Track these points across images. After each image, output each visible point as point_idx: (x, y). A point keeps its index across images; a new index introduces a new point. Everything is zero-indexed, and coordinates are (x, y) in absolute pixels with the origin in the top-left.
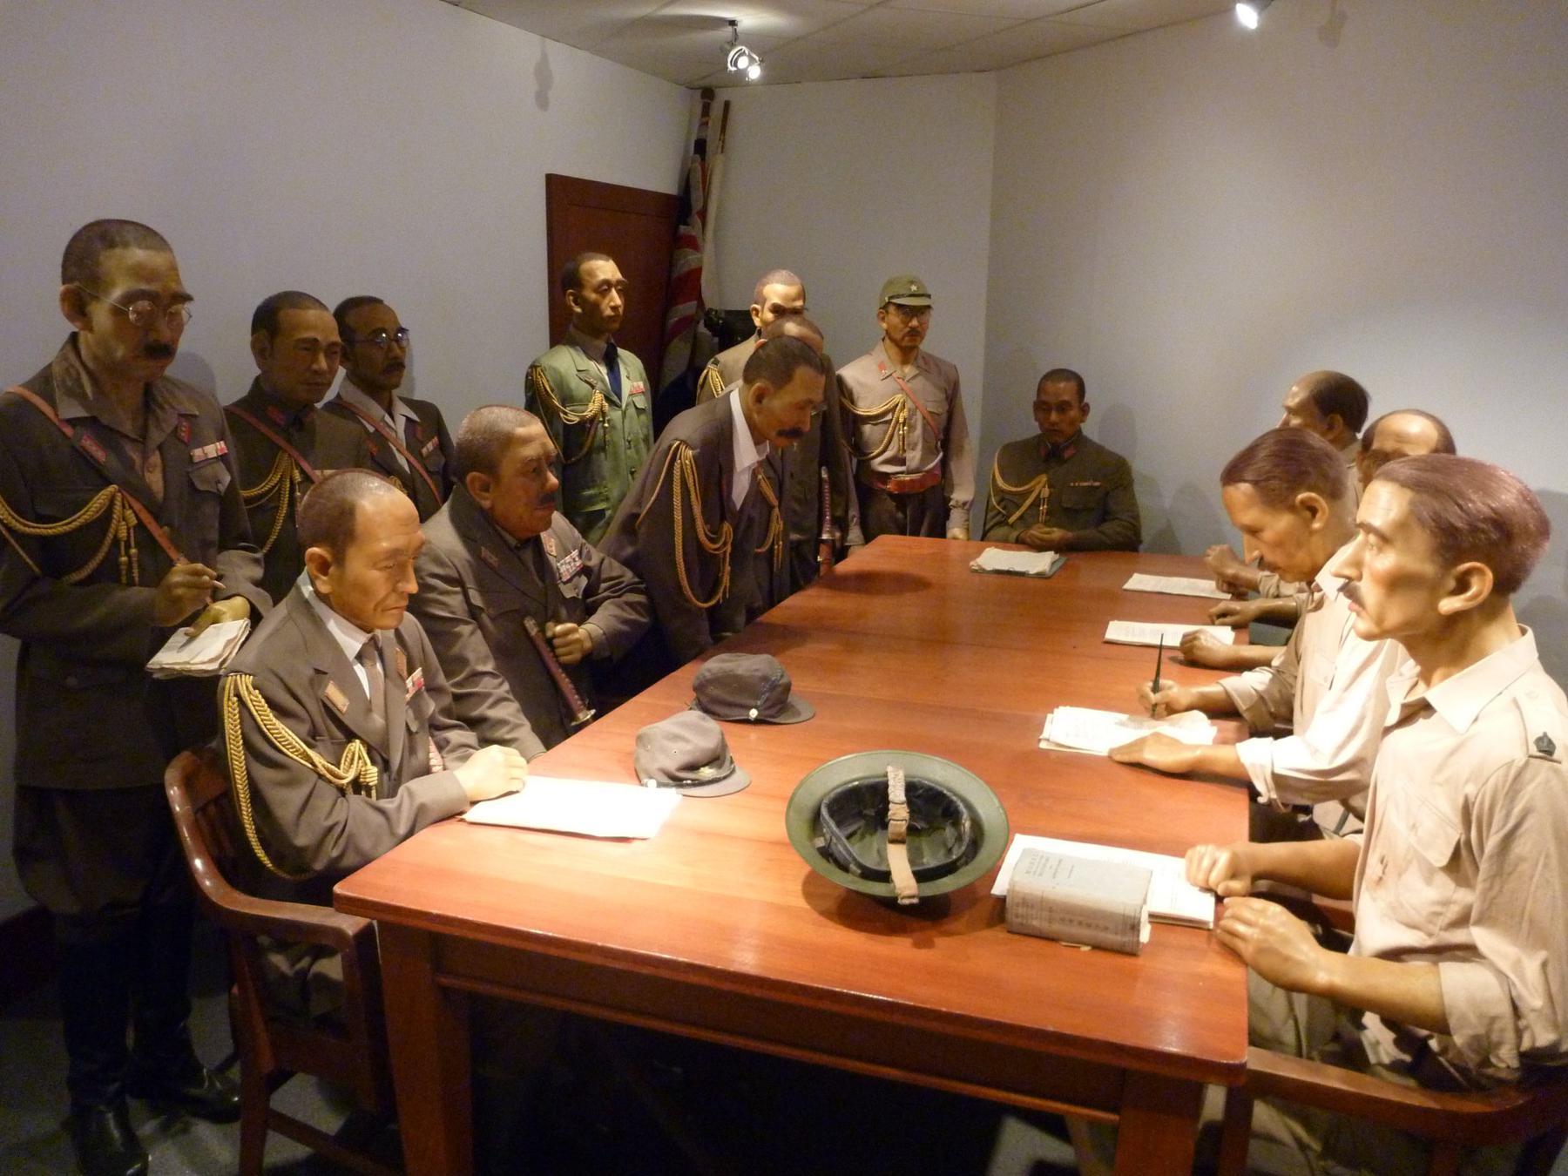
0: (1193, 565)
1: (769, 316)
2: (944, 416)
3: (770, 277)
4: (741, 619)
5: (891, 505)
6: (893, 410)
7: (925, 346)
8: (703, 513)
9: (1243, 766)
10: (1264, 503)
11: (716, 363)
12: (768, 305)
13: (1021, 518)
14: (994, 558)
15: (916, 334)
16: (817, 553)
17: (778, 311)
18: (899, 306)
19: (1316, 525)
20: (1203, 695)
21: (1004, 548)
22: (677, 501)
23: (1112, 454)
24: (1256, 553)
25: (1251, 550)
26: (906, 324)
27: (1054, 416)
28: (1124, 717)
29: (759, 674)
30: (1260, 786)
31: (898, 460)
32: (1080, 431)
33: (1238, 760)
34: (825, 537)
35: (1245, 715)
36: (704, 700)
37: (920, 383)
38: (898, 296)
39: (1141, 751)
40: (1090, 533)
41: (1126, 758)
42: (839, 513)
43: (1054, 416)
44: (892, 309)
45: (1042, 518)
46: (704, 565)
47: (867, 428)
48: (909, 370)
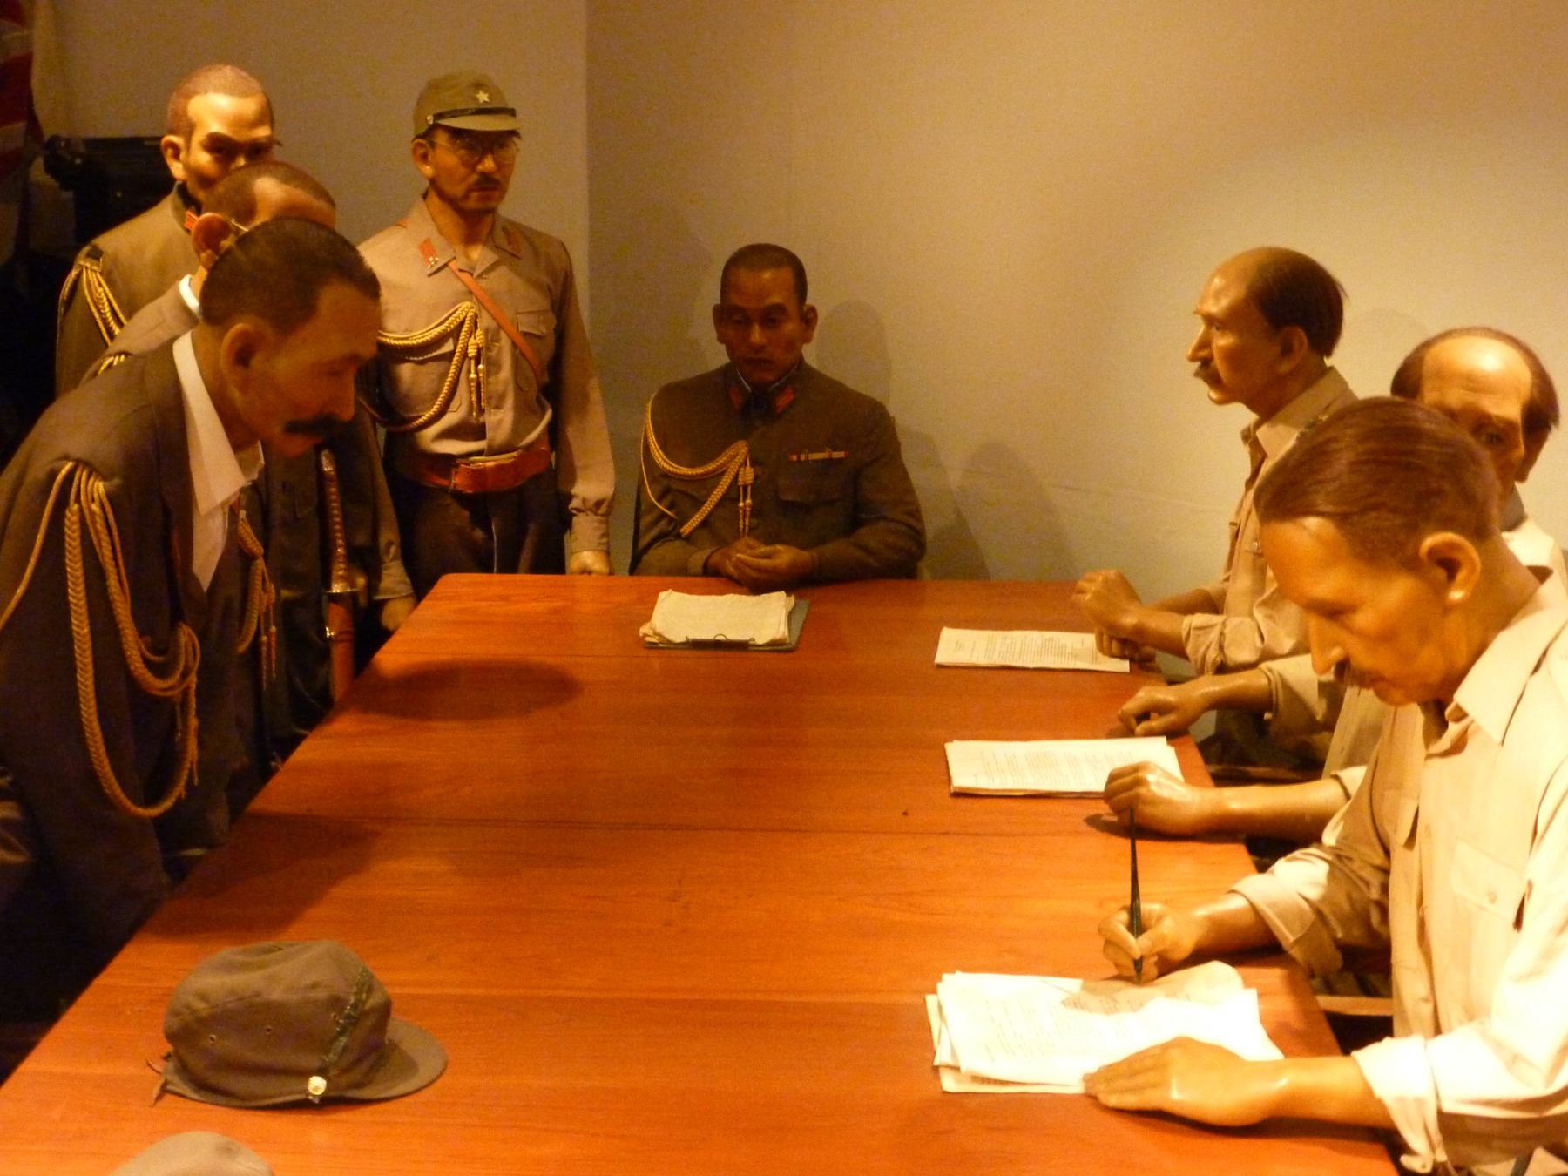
0: (1041, 598)
1: (203, 159)
2: (551, 341)
3: (201, 80)
4: (219, 817)
5: (461, 516)
6: (455, 333)
7: (510, 208)
8: (135, 616)
9: (1380, 1103)
10: (1358, 556)
11: (96, 255)
12: (199, 137)
13: (704, 524)
14: (684, 615)
15: (491, 186)
16: (321, 623)
17: (220, 147)
18: (456, 133)
19: (1457, 595)
20: (1215, 923)
21: (690, 592)
22: (77, 595)
23: (860, 400)
24: (1336, 653)
26: (472, 167)
27: (757, 335)
28: (1074, 985)
29: (321, 994)
30: (1415, 1140)
31: (470, 430)
32: (801, 359)
33: (1368, 1091)
34: (337, 588)
35: (1295, 953)
36: (197, 1064)
37: (501, 279)
38: (454, 114)
39: (1163, 1084)
40: (836, 549)
41: (1130, 1101)
42: (361, 539)
43: (757, 335)
44: (442, 139)
45: (744, 523)
46: (144, 725)
47: (406, 370)
48: (479, 254)
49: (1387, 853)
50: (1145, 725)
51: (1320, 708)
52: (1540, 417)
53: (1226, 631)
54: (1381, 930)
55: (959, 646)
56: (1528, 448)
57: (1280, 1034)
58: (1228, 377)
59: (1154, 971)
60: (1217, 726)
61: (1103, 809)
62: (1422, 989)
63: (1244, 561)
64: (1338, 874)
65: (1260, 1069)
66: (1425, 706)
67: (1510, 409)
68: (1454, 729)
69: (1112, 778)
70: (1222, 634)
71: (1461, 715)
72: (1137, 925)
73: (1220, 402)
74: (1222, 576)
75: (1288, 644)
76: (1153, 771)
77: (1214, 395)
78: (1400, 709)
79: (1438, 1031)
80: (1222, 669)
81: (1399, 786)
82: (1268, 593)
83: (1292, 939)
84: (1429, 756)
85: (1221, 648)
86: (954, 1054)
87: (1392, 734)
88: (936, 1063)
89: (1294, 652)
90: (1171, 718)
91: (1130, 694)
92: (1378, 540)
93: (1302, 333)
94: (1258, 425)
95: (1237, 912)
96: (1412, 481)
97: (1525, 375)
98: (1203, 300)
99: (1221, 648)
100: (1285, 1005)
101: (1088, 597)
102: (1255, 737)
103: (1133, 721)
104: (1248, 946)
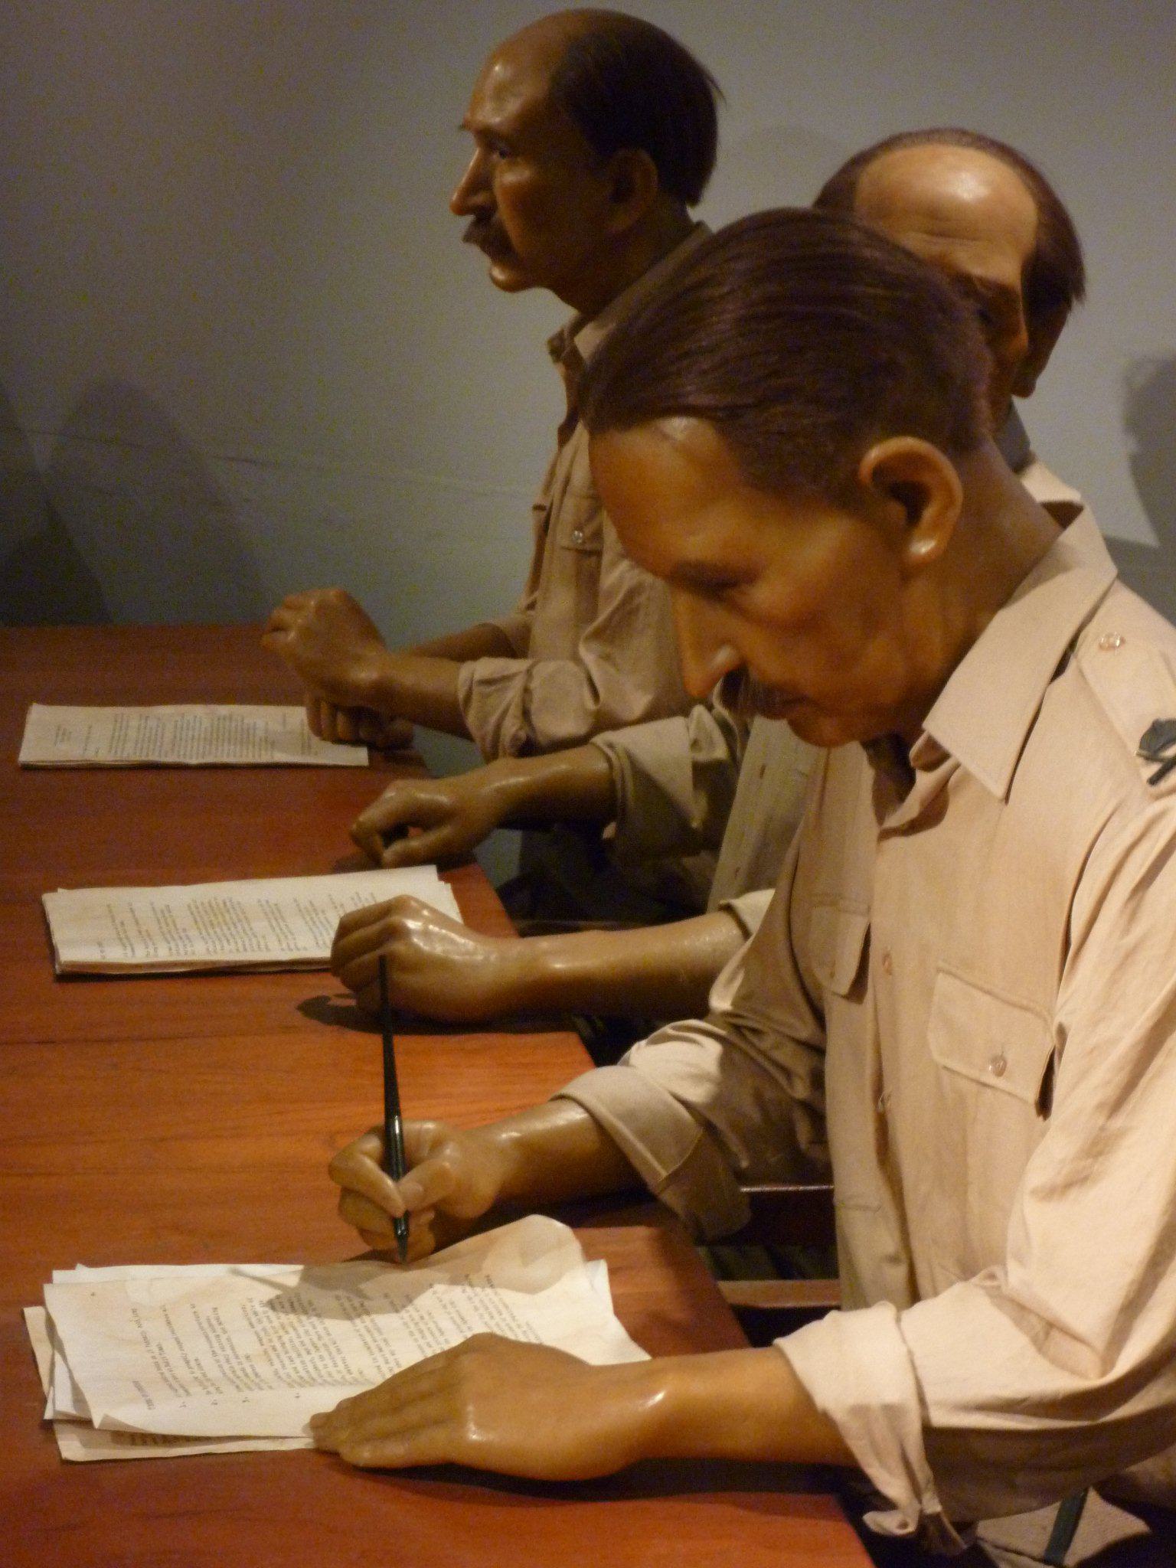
0: (216, 657)
9: (825, 1419)
19: (923, 547)
20: (531, 1150)
24: (723, 657)
25: (706, 646)
28: (288, 1274)
30: (891, 1483)
33: (805, 1400)
35: (670, 1197)
39: (453, 1418)
41: (395, 1452)
49: (819, 1017)
50: (398, 847)
51: (696, 809)
52: (1053, 280)
53: (534, 684)
54: (815, 1153)
55: (62, 733)
56: (1032, 339)
57: (647, 1328)
58: (521, 241)
59: (429, 1240)
60: (522, 867)
61: (331, 988)
62: (887, 1241)
63: (560, 564)
64: (737, 1057)
65: (614, 1376)
66: (871, 745)
67: (1003, 268)
68: (925, 781)
69: (346, 928)
70: (526, 691)
71: (937, 756)
72: (396, 1158)
73: (511, 287)
74: (524, 601)
75: (639, 702)
76: (415, 915)
77: (499, 274)
78: (837, 752)
79: (914, 1295)
80: (528, 748)
81: (833, 900)
82: (602, 617)
83: (664, 1174)
84: (886, 835)
85: (526, 714)
86: (78, 1397)
87: (819, 815)
88: (48, 1415)
89: (652, 715)
90: (445, 832)
91: (376, 793)
92: (786, 460)
93: (645, 156)
94: (577, 327)
95: (573, 1129)
96: (844, 390)
97: (1026, 209)
98: (476, 103)
99: (526, 714)
100: (656, 1284)
101: (292, 635)
102: (589, 853)
103: (378, 840)
104: (589, 1189)
